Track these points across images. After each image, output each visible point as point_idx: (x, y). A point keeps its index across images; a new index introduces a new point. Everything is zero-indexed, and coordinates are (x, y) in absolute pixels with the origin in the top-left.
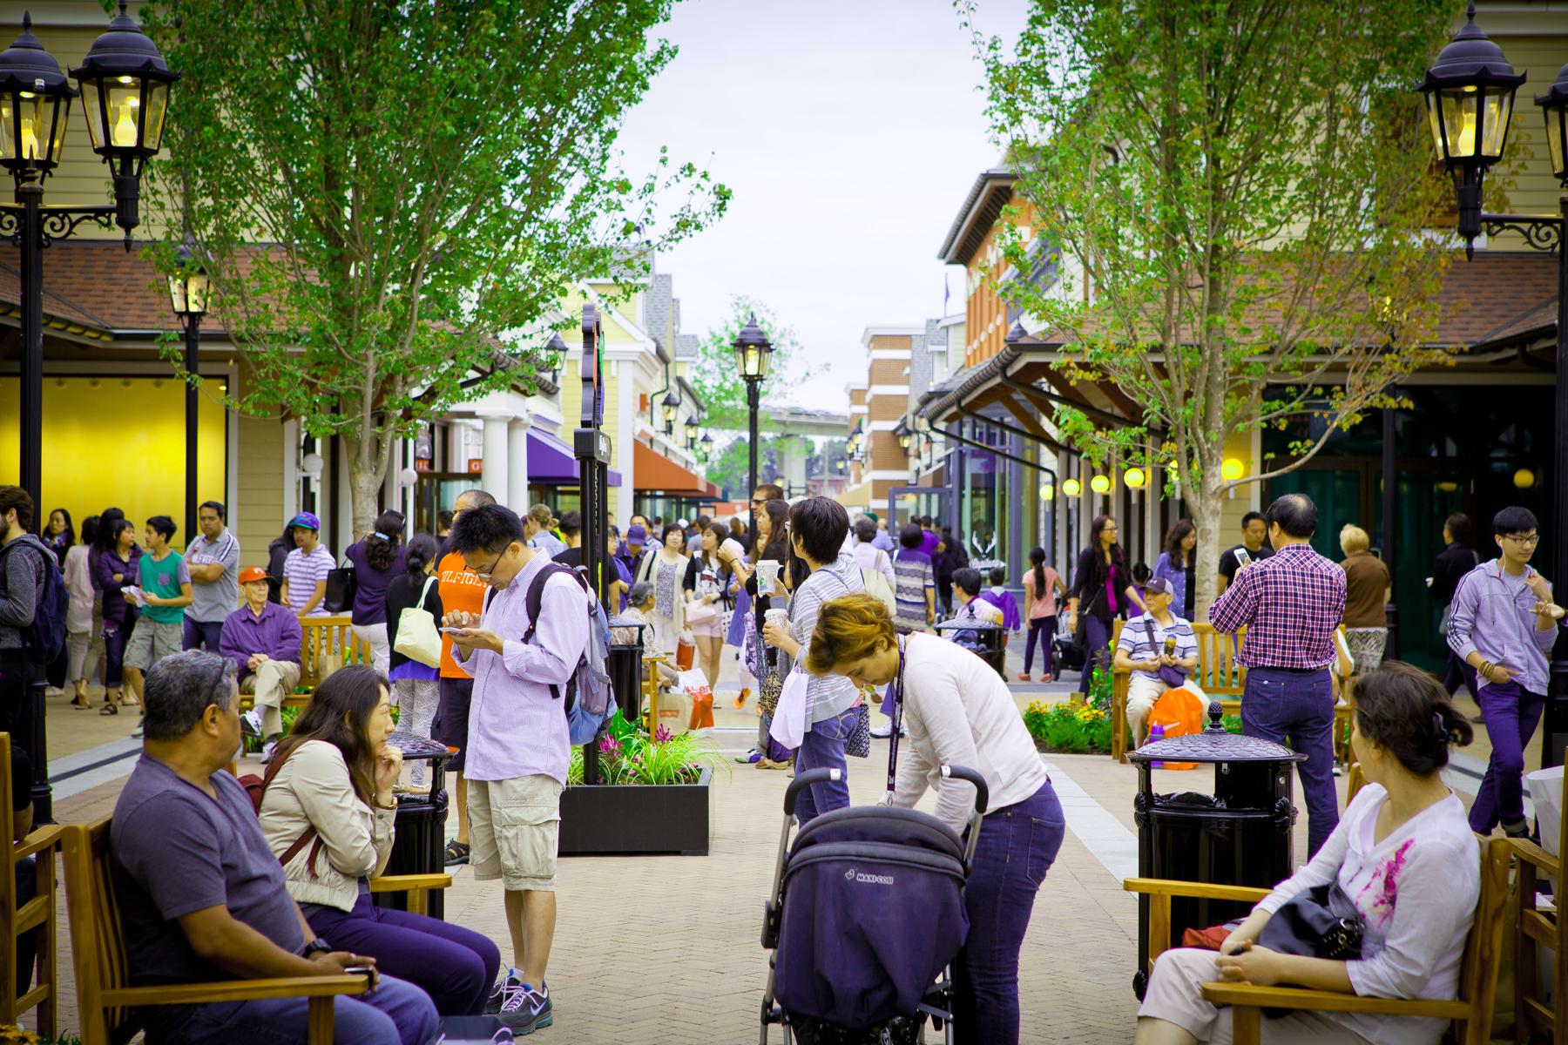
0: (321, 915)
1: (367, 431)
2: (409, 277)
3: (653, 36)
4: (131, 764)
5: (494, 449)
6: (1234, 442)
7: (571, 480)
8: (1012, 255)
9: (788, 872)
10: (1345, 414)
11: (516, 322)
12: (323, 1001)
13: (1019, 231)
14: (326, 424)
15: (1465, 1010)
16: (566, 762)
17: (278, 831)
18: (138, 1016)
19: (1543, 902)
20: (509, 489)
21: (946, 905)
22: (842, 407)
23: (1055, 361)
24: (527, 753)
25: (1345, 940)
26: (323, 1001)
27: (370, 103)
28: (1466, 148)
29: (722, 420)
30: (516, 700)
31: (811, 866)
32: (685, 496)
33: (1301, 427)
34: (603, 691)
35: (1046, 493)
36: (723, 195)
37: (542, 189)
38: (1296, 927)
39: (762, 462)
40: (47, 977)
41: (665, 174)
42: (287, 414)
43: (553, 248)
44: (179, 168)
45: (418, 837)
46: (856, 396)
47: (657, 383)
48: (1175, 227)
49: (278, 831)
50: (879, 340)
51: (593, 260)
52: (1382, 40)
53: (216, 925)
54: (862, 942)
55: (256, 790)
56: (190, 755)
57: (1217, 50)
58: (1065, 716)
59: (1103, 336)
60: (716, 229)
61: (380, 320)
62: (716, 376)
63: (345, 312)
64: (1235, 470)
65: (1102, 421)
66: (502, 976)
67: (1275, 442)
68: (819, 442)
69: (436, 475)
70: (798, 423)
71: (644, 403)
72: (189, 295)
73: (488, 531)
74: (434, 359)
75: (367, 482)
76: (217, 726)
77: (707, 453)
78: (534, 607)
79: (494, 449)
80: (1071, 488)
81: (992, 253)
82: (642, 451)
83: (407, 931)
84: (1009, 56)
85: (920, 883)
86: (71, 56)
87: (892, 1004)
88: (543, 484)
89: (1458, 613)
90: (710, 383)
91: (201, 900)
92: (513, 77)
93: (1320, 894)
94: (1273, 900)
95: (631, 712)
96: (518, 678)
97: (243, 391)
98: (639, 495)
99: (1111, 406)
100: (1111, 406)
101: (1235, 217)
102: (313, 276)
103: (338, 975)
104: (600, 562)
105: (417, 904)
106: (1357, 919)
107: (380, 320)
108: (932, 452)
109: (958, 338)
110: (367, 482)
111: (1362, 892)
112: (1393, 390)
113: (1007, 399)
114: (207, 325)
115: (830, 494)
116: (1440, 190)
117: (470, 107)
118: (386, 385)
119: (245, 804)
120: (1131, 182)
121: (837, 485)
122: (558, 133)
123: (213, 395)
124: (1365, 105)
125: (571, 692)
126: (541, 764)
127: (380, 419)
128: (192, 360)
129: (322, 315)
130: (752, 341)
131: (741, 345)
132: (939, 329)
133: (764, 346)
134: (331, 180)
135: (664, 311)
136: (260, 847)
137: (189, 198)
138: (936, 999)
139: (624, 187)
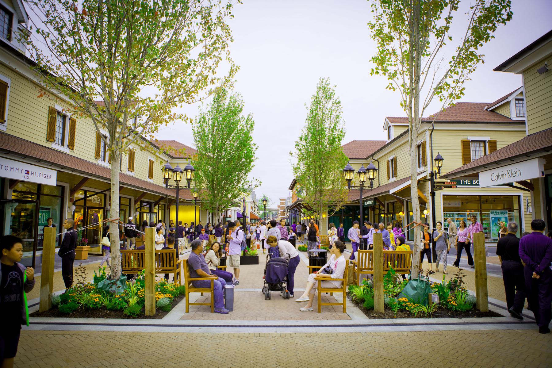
0: (212, 271)
1: (217, 212)
2: (222, 193)
3: (252, 164)
4: (190, 253)
5: (233, 214)
6: (325, 213)
7: (242, 217)
8: (297, 190)
9: (267, 266)
10: (337, 209)
11: (235, 198)
12: (212, 280)
13: (298, 186)
14: (212, 211)
15: (344, 280)
16: (241, 253)
17: (207, 260)
18: (192, 282)
19: (356, 268)
20: (234, 219)
21: (286, 270)
22: (276, 208)
23: (302, 203)
24: (235, 252)
25: (331, 272)
26: (212, 280)
27: (218, 172)
28: (348, 178)
29: (261, 210)
30: (235, 245)
31: (270, 265)
32: (257, 219)
33: (332, 211)
34: (245, 244)
35: (302, 219)
36: (261, 183)
37: (239, 182)
38: (325, 271)
39: (266, 215)
40: (180, 278)
41: (254, 180)
42: (207, 210)
43: (240, 189)
44: (195, 180)
45: (223, 262)
46: (278, 206)
47: (253, 205)
48: (316, 186)
49: (207, 260)
50: (281, 199)
51: (245, 191)
52: (340, 164)
53: (200, 271)
54: (276, 274)
55: (205, 256)
56: (197, 251)
57: (321, 165)
58: (303, 247)
59: (308, 200)
60: (260, 187)
61: (219, 198)
62: (260, 204)
63: (214, 197)
64: (325, 216)
65: (309, 210)
66: (233, 279)
67: (329, 213)
68: (274, 212)
69: (225, 217)
70: (270, 210)
71: (251, 208)
72: (196, 195)
73: (232, 225)
74: (225, 203)
75: (217, 218)
76: (199, 248)
77: (259, 214)
78: (237, 234)
79: (233, 214)
80: (305, 218)
81: (294, 190)
82: (251, 214)
83: (222, 273)
84: (296, 166)
85: (282, 267)
86: (183, 167)
87: (279, 281)
88: (239, 218)
89: (349, 234)
90: (260, 205)
91: (199, 268)
92: (235, 169)
93: (328, 267)
94: (322, 268)
95: (249, 246)
96: (235, 243)
97: (202, 207)
98: (251, 219)
99: (308, 208)
100: (308, 208)
101: (324, 185)
102: (211, 193)
103: (214, 277)
104: (244, 228)
105: (223, 270)
106: (332, 270)
107: (219, 198)
108: (288, 214)
109: (291, 199)
110: (217, 218)
111: (333, 267)
112: (343, 206)
113: (297, 207)
114: (197, 199)
115: (275, 219)
116: (347, 183)
117: (230, 172)
118: (219, 206)
119: (203, 257)
120: (311, 181)
121: (276, 218)
122: (240, 175)
123: (198, 207)
124: (338, 172)
125: (242, 244)
126: (238, 253)
127: (218, 210)
128: (196, 203)
129: (212, 197)
130: (265, 200)
131: (263, 201)
132: (289, 198)
133: (266, 201)
134: (213, 181)
135: (254, 196)
136: (205, 262)
137: (196, 184)
138: (285, 281)
139: (248, 182)
